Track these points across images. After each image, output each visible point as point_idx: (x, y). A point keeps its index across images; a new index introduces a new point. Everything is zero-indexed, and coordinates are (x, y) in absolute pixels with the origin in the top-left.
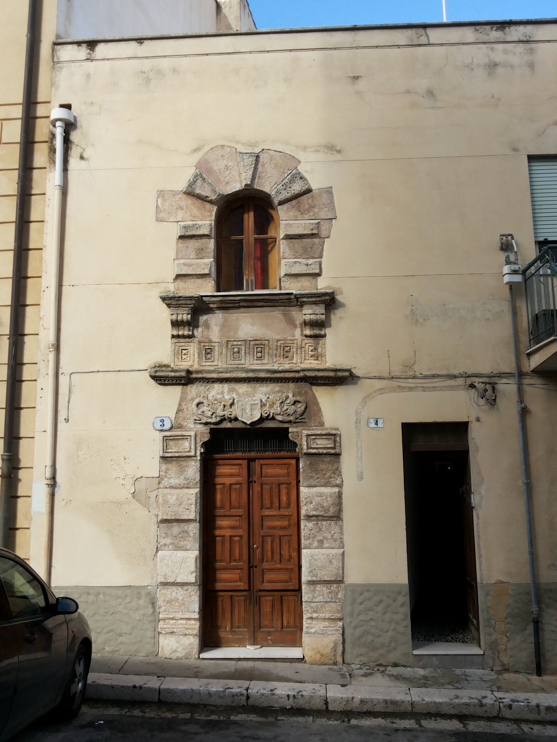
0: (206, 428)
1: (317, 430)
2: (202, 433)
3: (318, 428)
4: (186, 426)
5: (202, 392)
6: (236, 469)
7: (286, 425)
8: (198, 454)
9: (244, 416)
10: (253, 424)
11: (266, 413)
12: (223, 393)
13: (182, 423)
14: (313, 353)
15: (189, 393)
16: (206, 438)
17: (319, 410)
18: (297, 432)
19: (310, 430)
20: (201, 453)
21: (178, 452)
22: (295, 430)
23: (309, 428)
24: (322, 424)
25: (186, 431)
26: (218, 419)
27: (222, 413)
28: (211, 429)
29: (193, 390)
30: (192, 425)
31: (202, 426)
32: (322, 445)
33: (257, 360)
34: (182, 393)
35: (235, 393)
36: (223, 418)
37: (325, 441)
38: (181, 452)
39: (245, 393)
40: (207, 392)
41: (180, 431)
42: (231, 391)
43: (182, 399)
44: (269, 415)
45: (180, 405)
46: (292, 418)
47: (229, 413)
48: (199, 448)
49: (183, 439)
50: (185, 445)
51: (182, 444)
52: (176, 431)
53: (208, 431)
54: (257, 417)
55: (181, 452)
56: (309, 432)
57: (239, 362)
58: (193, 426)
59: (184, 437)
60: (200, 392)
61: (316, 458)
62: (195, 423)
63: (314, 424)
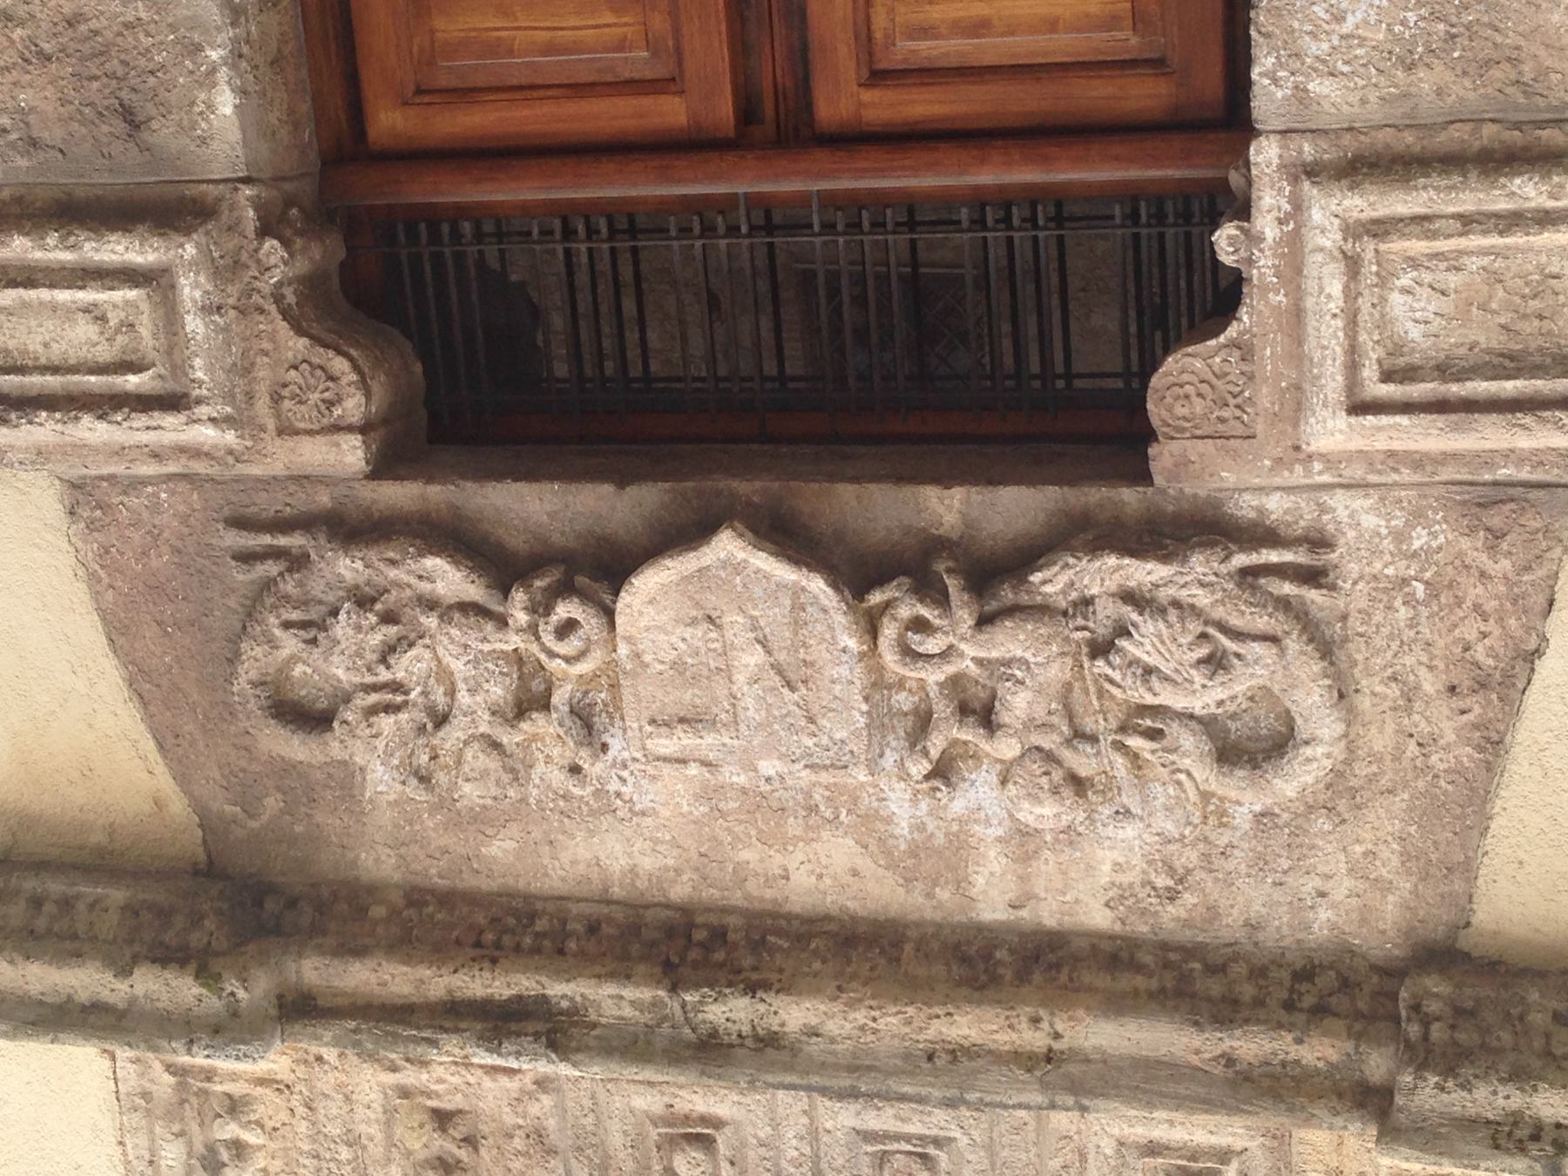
0: (1196, 488)
1: (120, 452)
2: (1232, 435)
3: (118, 469)
4: (1417, 516)
5: (1238, 861)
6: (926, 32)
7: (399, 494)
8: (1269, 201)
9: (774, 616)
10: (685, 533)
11: (567, 628)
12: (1024, 842)
13: (1472, 548)
14: (229, 1130)
15: (1389, 864)
16: (1184, 378)
17: (118, 631)
18: (286, 430)
19: (182, 450)
20: (1243, 210)
21: (1513, 221)
22: (316, 454)
23: (191, 474)
24: (85, 498)
25: (1418, 461)
26: (1053, 582)
27: (1010, 641)
28: (1143, 476)
29: (1339, 889)
30: (1357, 518)
31: (1245, 507)
32: (54, 307)
33: (718, 1124)
34: (1467, 869)
35: (903, 828)
36: (1007, 595)
37: (34, 345)
38: (1468, 222)
39: (794, 826)
40: (1190, 857)
41: (1486, 459)
42: (952, 855)
43: (1468, 801)
44: (541, 608)
45: (1492, 744)
46: (349, 567)
47: (932, 645)
48: (1264, 268)
49: (1444, 370)
50: (1429, 304)
51: (1461, 316)
52: (1536, 458)
53: (1162, 456)
54: (650, 593)
55: (1468, 222)
56: (171, 429)
57: (881, 1119)
58: (1341, 503)
59: (1429, 385)
60: (1261, 863)
61: (99, 179)
62: (1319, 541)
63: (155, 508)
